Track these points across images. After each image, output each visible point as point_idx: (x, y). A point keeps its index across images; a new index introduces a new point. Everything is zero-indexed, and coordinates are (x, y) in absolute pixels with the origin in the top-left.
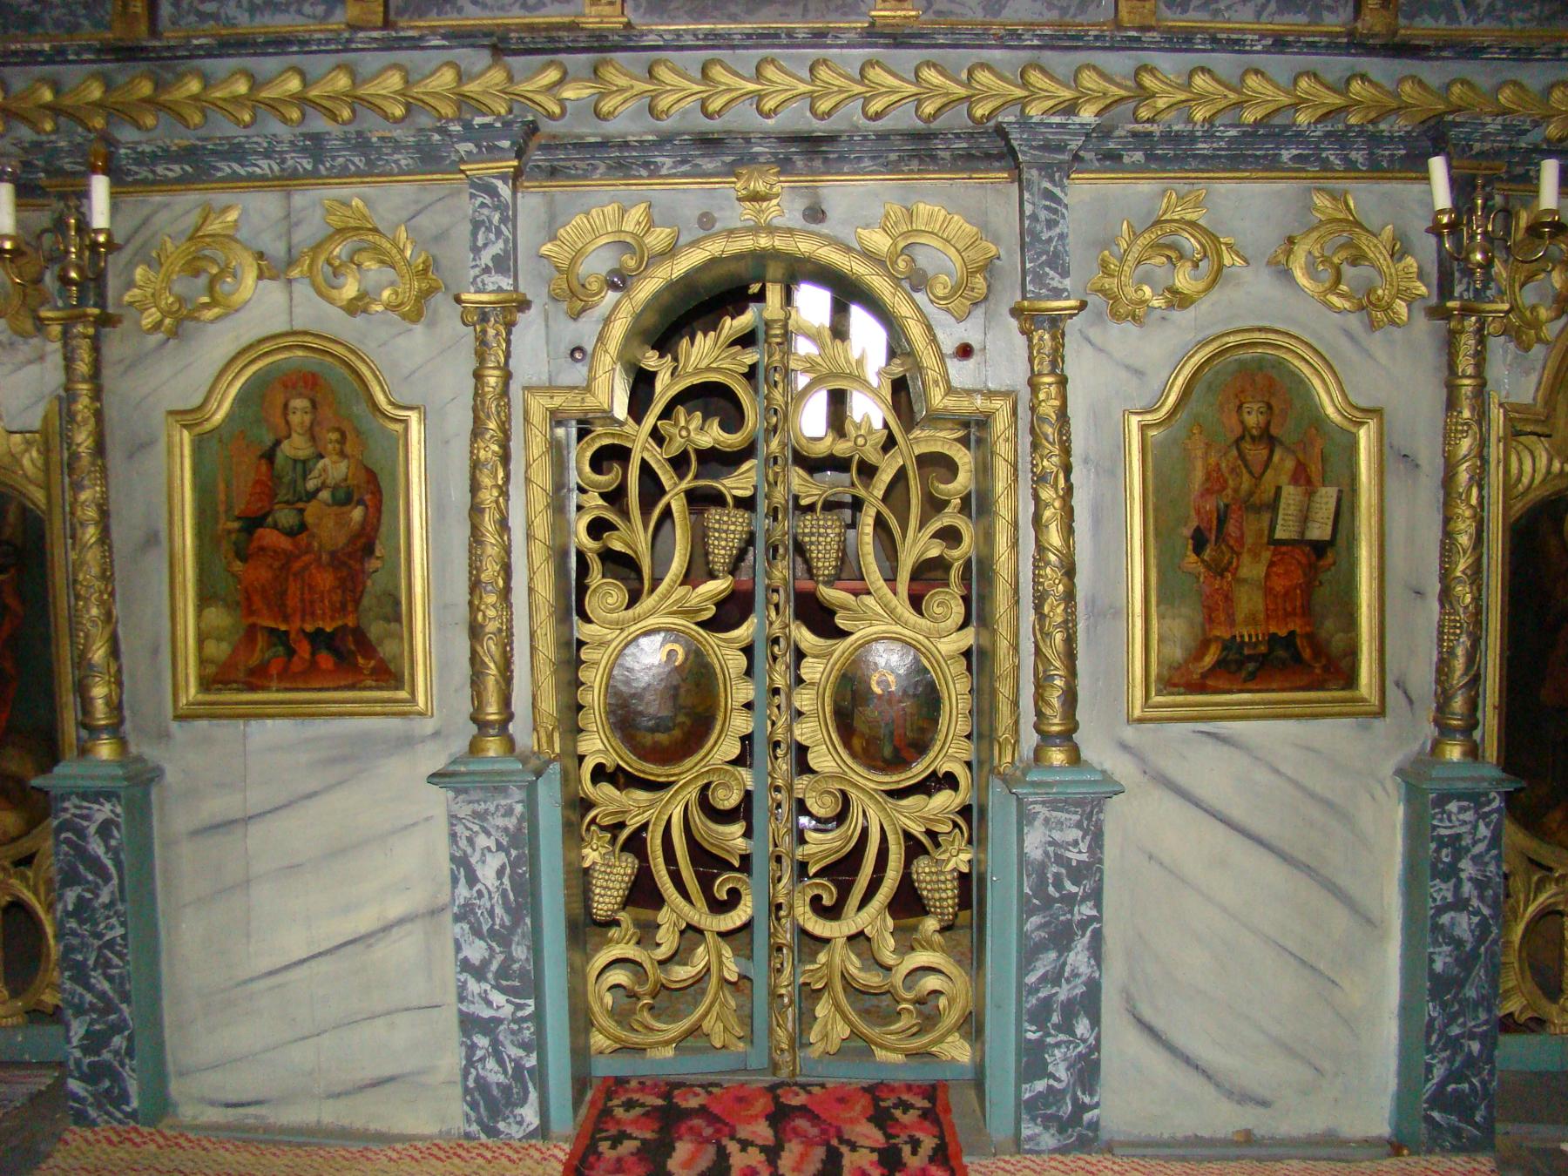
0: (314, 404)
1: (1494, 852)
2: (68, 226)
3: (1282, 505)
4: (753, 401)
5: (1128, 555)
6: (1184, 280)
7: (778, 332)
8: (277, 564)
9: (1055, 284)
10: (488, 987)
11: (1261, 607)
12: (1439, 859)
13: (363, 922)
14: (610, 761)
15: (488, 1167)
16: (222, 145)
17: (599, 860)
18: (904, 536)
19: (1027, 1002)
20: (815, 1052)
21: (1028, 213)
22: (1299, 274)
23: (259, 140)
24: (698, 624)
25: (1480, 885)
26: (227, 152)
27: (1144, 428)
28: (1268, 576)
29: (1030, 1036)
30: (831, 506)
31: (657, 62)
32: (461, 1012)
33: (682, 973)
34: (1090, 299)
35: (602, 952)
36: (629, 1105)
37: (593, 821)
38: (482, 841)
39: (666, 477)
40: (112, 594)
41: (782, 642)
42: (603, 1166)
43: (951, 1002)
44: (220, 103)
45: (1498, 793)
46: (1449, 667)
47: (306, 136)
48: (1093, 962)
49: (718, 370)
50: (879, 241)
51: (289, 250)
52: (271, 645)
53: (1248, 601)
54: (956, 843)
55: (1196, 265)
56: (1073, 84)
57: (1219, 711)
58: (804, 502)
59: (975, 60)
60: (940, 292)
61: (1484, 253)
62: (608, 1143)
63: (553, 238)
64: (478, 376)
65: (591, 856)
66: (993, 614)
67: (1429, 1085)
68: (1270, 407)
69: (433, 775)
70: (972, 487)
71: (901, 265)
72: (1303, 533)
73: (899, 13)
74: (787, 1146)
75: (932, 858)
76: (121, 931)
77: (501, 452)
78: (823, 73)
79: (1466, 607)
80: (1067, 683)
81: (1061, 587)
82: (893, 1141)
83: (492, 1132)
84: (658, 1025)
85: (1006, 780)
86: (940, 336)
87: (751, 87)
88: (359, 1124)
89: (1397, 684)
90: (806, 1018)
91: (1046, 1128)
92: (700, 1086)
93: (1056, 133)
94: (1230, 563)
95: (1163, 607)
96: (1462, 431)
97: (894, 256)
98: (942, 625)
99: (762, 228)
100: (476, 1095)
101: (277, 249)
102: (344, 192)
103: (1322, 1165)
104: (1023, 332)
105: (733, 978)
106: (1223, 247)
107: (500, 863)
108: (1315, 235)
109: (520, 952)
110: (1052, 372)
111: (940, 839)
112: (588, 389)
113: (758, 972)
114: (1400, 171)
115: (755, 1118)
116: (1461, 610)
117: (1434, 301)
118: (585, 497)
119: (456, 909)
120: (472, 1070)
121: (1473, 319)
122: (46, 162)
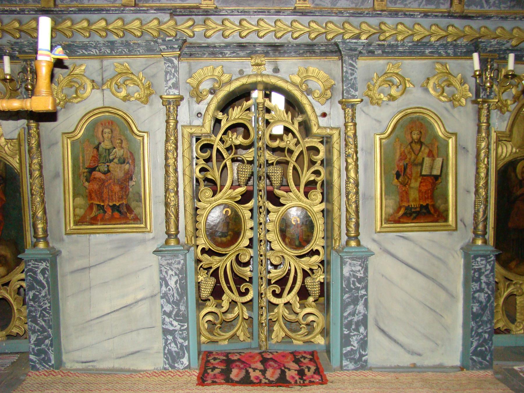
0: (112, 131)
1: (492, 274)
2: (27, 70)
3: (425, 164)
5: (375, 179)
6: (394, 91)
7: (261, 106)
8: (100, 184)
9: (353, 93)
10: (172, 320)
11: (417, 196)
12: (474, 276)
13: (129, 300)
15: (172, 378)
16: (80, 44)
17: (203, 280)
18: (302, 173)
19: (344, 322)
20: (274, 341)
21: (344, 71)
22: (431, 90)
23: (93, 43)
24: (235, 202)
25: (488, 284)
26: (81, 46)
27: (381, 139)
28: (420, 186)
29: (345, 332)
30: (278, 163)
31: (225, 19)
32: (163, 328)
33: (230, 316)
34: (363, 98)
35: (204, 310)
36: (215, 359)
37: (201, 267)
38: (170, 272)
39: (225, 154)
40: (44, 194)
41: (263, 207)
42: (210, 376)
43: (318, 325)
44: (78, 30)
45: (493, 255)
46: (478, 215)
47: (108, 42)
48: (365, 309)
49: (241, 119)
50: (297, 80)
51: (103, 79)
52: (98, 210)
53: (414, 194)
54: (319, 273)
55: (398, 87)
56: (359, 28)
57: (404, 229)
58: (270, 162)
59: (327, 20)
60: (316, 95)
61: (490, 83)
62: (211, 370)
63: (191, 77)
64: (167, 122)
65: (201, 278)
66: (332, 199)
67: (472, 348)
68: (421, 132)
69: (154, 251)
70: (324, 157)
71: (304, 87)
72: (431, 172)
73: (304, 5)
74: (268, 370)
76: (49, 305)
77: (175, 147)
78: (279, 24)
79: (483, 196)
80: (356, 220)
81: (354, 190)
82: (301, 368)
83: (173, 367)
84: (222, 334)
85: (337, 251)
86: (316, 110)
87: (256, 28)
88: (127, 367)
89: (461, 220)
90: (270, 331)
91: (351, 362)
92: (238, 353)
93: (353, 45)
94: (408, 182)
95: (386, 196)
96: (482, 140)
97: (302, 83)
98: (315, 202)
99: (259, 74)
100: (168, 355)
101: (98, 79)
102: (121, 60)
103: (438, 374)
104: (343, 109)
105: (247, 317)
106: (407, 81)
107: (176, 279)
108: (436, 77)
109: (182, 308)
110: (352, 122)
111: (314, 271)
112: (203, 126)
113: (255, 315)
114: (463, 56)
115: (257, 362)
116: (481, 197)
117: (474, 98)
118: (198, 160)
119: (161, 295)
120: (167, 347)
121: (486, 104)
122: (20, 49)
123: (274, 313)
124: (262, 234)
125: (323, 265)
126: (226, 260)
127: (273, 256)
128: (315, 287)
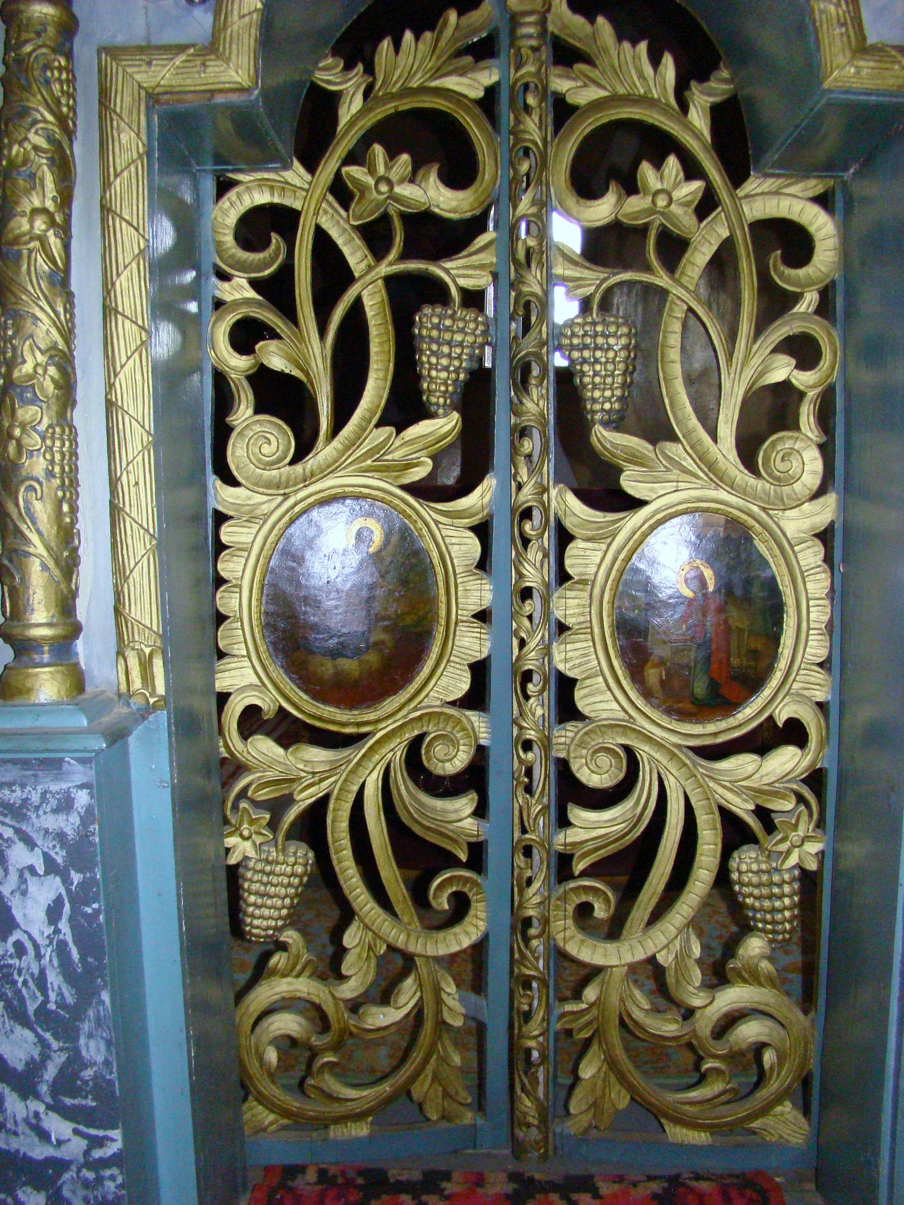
4: (490, 142)
7: (531, 30)
10: (42, 1108)
14: (268, 702)
17: (251, 853)
24: (404, 488)
37: (243, 794)
41: (536, 514)
43: (781, 1058)
75: (762, 849)
107: (52, 896)
123: (584, 1006)
124: (532, 644)
125: (819, 793)
126: (359, 764)
127: (581, 744)
128: (776, 890)
